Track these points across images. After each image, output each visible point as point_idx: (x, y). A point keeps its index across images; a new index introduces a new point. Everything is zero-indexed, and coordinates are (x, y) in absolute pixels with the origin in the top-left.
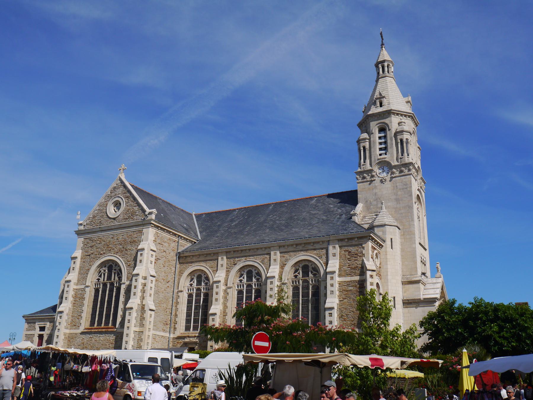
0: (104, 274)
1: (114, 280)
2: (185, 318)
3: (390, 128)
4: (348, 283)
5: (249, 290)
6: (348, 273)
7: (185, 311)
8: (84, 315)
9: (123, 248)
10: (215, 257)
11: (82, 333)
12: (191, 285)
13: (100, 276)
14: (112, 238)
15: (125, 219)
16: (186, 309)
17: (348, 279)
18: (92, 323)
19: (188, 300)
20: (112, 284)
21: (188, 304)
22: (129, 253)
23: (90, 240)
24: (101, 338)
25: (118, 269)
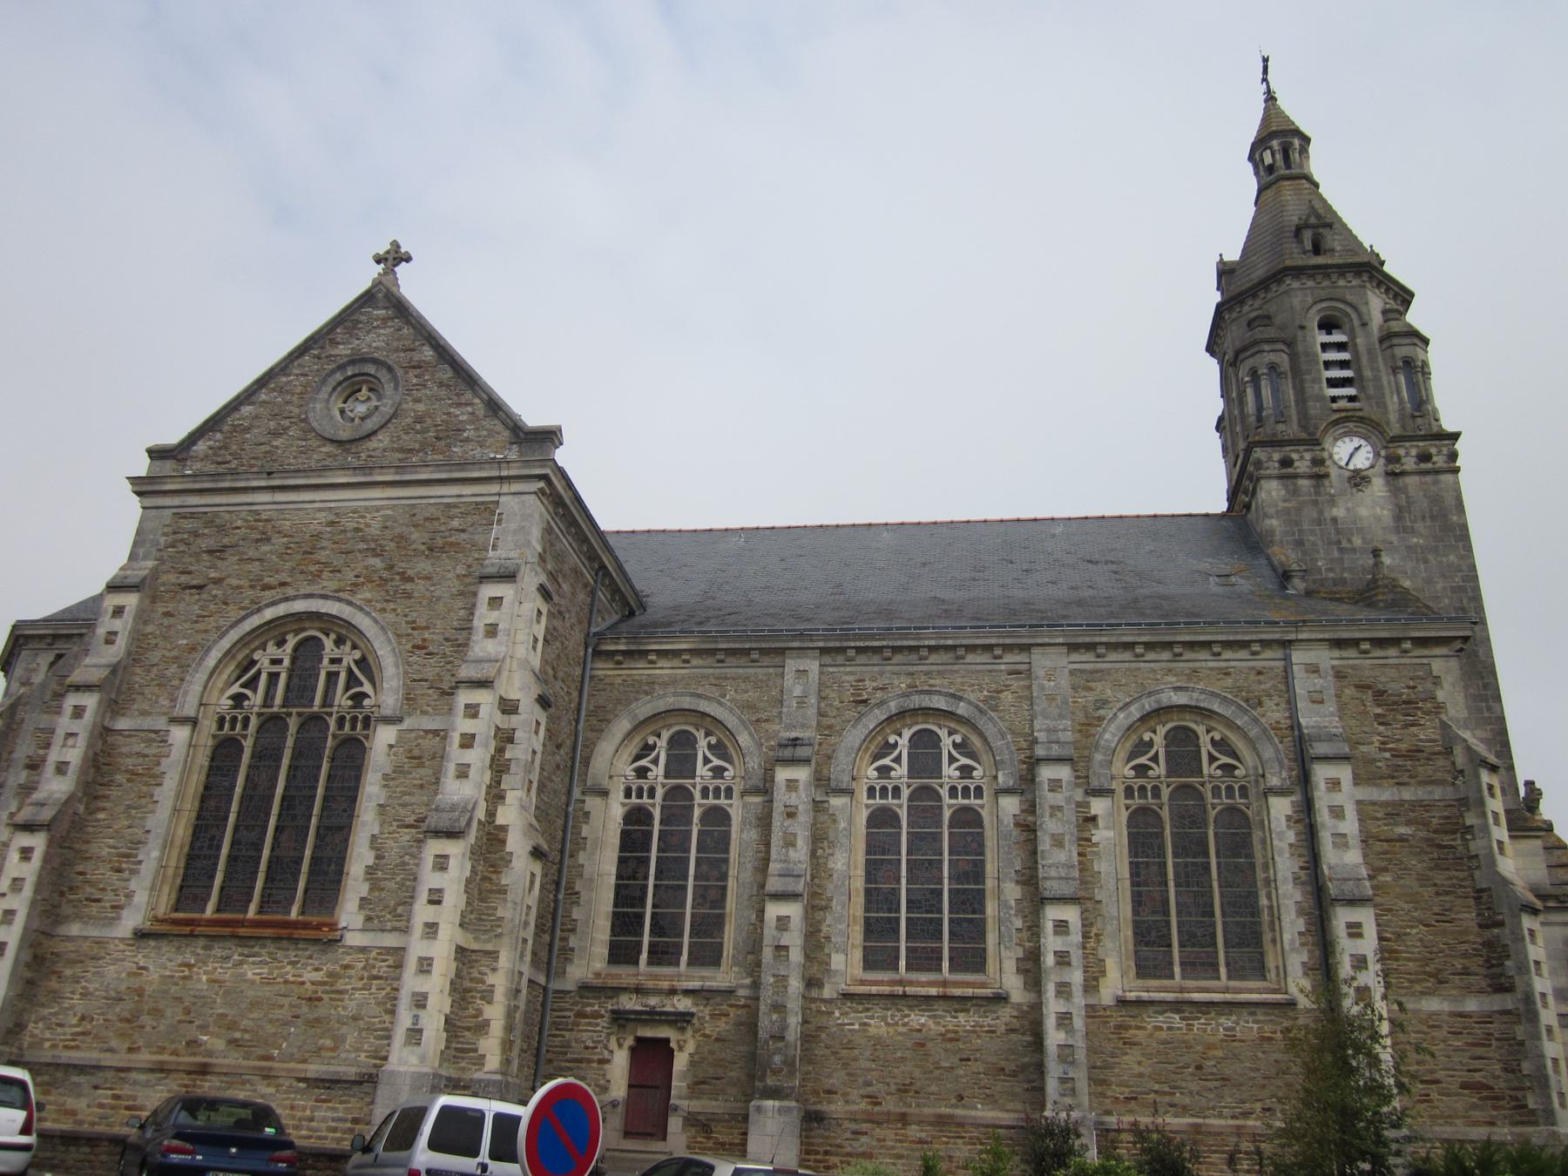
0: (273, 677)
1: (327, 701)
2: (610, 909)
3: (1366, 317)
4: (1394, 811)
5: (925, 809)
6: (1385, 771)
7: (613, 880)
8: (151, 856)
9: (390, 567)
10: (777, 660)
11: (141, 935)
12: (642, 773)
13: (252, 684)
14: (332, 524)
15: (401, 450)
16: (614, 870)
17: (1387, 794)
18: (190, 890)
19: (623, 832)
20: (314, 722)
21: (623, 848)
22: (419, 587)
23: (210, 523)
24: (250, 972)
25: (349, 657)
